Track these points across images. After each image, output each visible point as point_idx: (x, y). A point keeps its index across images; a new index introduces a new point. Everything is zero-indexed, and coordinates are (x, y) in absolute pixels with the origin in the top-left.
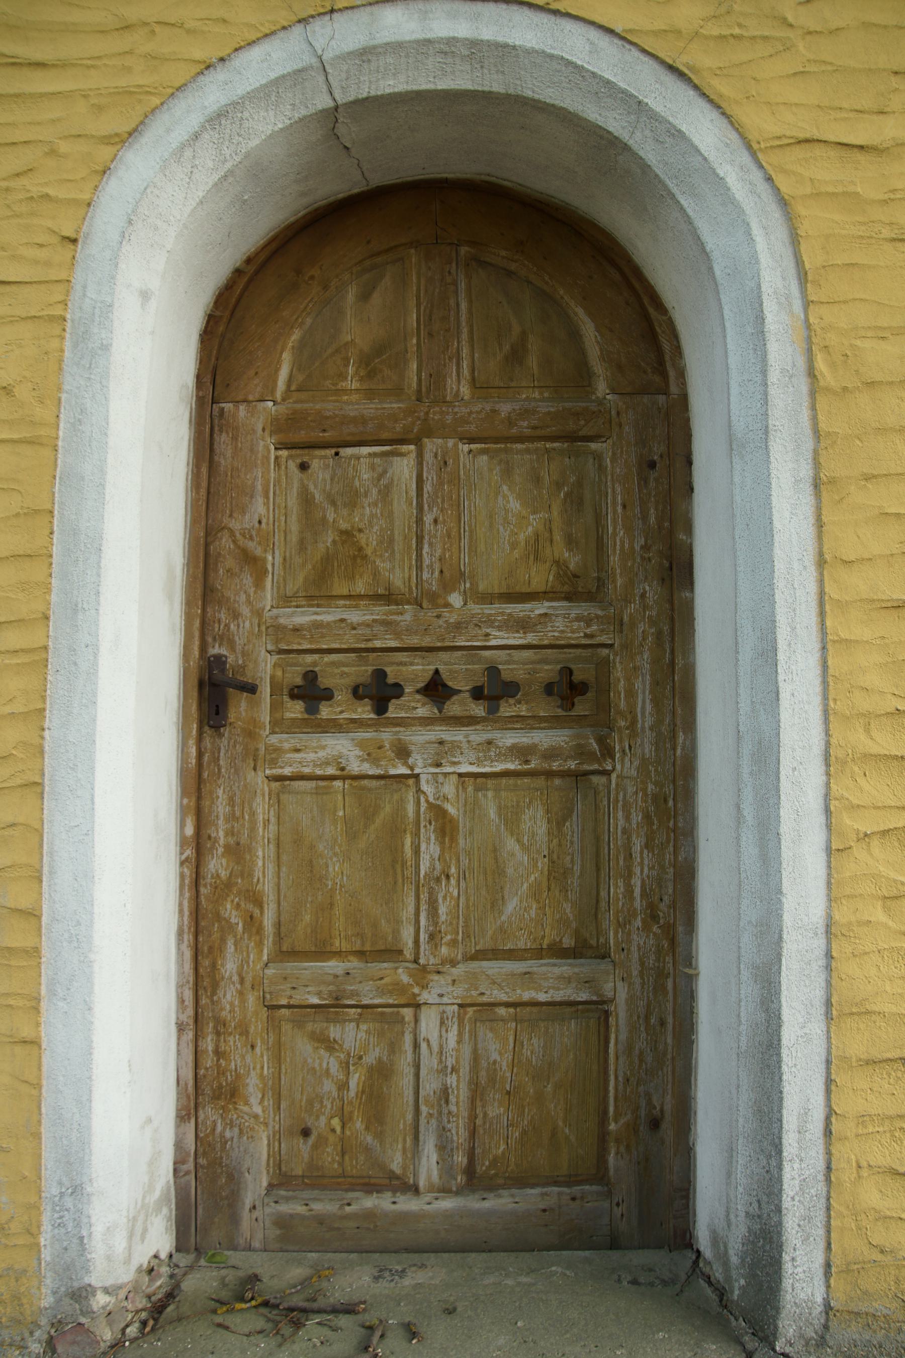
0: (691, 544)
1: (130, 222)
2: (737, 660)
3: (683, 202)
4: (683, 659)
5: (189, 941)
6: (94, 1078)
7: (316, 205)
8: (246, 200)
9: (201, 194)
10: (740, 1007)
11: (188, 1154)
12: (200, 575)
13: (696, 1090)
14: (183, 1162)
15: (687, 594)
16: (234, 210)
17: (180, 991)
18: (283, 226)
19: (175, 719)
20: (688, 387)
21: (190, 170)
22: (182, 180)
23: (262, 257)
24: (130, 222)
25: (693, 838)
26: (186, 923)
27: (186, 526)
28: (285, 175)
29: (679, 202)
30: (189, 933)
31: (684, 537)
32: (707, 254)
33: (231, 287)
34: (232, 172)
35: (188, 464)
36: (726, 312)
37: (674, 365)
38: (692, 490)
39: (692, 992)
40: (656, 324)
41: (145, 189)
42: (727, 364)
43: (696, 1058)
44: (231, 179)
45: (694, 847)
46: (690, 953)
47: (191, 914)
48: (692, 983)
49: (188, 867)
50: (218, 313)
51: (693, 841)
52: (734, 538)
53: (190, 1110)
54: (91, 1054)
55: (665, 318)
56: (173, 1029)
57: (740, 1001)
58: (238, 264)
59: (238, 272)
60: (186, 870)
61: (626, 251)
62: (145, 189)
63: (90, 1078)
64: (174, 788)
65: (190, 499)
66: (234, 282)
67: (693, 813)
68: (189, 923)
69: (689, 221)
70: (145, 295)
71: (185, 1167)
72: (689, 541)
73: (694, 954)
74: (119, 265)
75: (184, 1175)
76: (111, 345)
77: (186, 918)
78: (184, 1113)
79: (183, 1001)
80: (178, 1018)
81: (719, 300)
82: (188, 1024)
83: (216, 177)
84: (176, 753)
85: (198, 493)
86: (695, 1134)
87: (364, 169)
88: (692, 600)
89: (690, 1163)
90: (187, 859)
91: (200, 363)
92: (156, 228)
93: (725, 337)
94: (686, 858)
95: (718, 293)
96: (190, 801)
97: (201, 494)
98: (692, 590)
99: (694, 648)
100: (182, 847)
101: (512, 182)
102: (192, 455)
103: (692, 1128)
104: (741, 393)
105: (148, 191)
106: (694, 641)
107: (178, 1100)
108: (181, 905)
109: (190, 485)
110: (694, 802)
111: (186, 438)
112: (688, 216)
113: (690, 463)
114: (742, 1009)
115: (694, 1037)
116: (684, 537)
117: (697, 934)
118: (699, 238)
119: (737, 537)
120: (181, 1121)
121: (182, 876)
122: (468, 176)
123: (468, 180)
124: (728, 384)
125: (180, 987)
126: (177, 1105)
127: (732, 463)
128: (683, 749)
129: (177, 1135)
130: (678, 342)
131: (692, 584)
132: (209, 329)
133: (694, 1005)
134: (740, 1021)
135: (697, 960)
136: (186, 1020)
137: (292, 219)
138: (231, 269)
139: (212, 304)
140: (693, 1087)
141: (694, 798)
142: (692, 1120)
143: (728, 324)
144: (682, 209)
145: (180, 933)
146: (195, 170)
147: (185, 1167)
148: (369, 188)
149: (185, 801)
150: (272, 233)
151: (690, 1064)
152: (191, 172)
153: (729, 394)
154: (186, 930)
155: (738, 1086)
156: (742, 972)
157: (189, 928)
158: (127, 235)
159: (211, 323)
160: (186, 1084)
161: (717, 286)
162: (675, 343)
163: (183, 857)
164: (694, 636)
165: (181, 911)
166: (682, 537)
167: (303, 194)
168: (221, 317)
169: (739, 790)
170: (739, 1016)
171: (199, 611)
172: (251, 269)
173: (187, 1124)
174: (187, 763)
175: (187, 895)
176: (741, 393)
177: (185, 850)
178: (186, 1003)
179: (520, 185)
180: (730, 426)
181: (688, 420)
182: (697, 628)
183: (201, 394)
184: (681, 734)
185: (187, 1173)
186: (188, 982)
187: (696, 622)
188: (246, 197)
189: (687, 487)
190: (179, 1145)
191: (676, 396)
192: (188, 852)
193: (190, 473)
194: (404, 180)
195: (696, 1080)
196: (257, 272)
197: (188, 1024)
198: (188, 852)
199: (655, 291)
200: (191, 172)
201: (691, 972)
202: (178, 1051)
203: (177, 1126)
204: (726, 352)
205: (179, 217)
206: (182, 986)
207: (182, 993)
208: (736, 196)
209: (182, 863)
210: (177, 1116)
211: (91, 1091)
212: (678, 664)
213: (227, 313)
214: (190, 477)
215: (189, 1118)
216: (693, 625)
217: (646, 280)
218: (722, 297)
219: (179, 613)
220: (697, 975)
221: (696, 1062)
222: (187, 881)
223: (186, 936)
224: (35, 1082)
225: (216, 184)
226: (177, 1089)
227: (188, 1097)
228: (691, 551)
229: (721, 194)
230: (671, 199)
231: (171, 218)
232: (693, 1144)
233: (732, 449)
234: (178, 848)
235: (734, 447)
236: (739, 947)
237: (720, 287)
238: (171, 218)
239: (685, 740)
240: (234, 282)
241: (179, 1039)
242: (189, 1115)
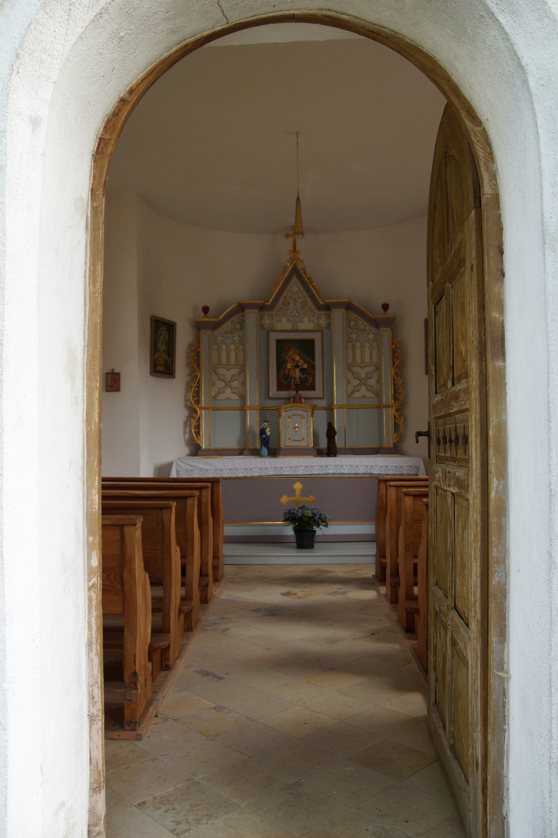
0: (503, 321)
1: (17, 56)
2: (550, 428)
3: (501, 20)
4: (496, 418)
5: (97, 650)
6: (8, 786)
7: (185, 42)
8: (123, 37)
9: (80, 30)
10: (551, 724)
11: (99, 819)
12: (98, 355)
13: (508, 771)
14: (96, 825)
15: (500, 364)
16: (112, 45)
17: (90, 689)
18: (158, 61)
19: (80, 474)
20: (499, 187)
21: (68, 7)
22: (62, 17)
23: (142, 88)
24: (17, 56)
25: (505, 565)
26: (94, 636)
27: (85, 315)
28: (155, 14)
29: (497, 20)
30: (96, 644)
31: (497, 316)
32: (522, 68)
33: (118, 114)
34: (106, 9)
35: (86, 264)
36: (540, 120)
37: (487, 169)
38: (503, 275)
39: (504, 690)
40: (472, 134)
41: (29, 25)
42: (540, 167)
43: (508, 744)
44: (106, 17)
45: (506, 573)
46: (502, 659)
47: (98, 629)
48: (504, 683)
49: (94, 592)
50: (107, 137)
51: (505, 568)
52: (546, 321)
53: (100, 784)
54: (6, 767)
55: (479, 129)
56: (86, 720)
57: (552, 719)
58: (122, 95)
59: (123, 101)
60: (93, 594)
61: (446, 72)
62: (29, 25)
63: (5, 787)
64: (81, 530)
65: (88, 292)
66: (120, 110)
67: (505, 545)
68: (97, 636)
69: (506, 37)
70: (35, 122)
71: (97, 829)
72: (501, 318)
73: (505, 660)
74: (10, 95)
75: (97, 835)
76: (6, 166)
77: (94, 632)
78: (95, 786)
79: (93, 698)
80: (89, 711)
81: (533, 109)
82: (97, 716)
83: (92, 14)
84: (81, 501)
85: (94, 287)
86: (508, 806)
87: (223, 7)
88: (504, 368)
89: (504, 830)
90: (93, 585)
91: (94, 179)
92: (42, 62)
93: (538, 142)
94: (499, 582)
95: (532, 103)
96: (95, 539)
97: (97, 287)
98: (504, 360)
99: (505, 408)
100: (89, 575)
101: (349, 15)
102: (89, 255)
103: (505, 800)
104: (553, 193)
105: (32, 27)
106: (505, 402)
107: (91, 776)
108: (89, 622)
109: (87, 281)
110: (505, 536)
111: (83, 242)
112: (506, 33)
113: (501, 252)
114: (554, 726)
115: (505, 727)
116: (497, 316)
117: (508, 644)
118: (515, 53)
119: (549, 320)
120: (93, 792)
121: (90, 599)
122: (312, 12)
123: (312, 15)
124: (541, 185)
125: (91, 686)
126: (90, 780)
127: (544, 255)
128: (497, 492)
129: (90, 803)
130: (491, 149)
131: (503, 354)
132: (100, 150)
133: (506, 700)
134: (552, 736)
135: (508, 665)
136: (96, 712)
137: (166, 55)
138: (117, 99)
139: (102, 129)
140: (505, 767)
141: (505, 532)
142: (505, 795)
143: (541, 131)
144: (501, 28)
145: (90, 644)
146: (73, 8)
147: (97, 829)
148: (229, 25)
149: (91, 539)
150: (150, 67)
151: (502, 749)
152: (70, 10)
153: (542, 194)
154: (94, 642)
155: (551, 791)
156: (553, 695)
157: (97, 640)
158: (15, 68)
159: (102, 145)
160: (97, 763)
161: (531, 97)
162: (488, 150)
163: (91, 584)
164: (505, 397)
165: (90, 627)
166: (495, 315)
167: (173, 32)
168: (110, 139)
169: (551, 540)
170: (550, 731)
171: (98, 384)
172: (134, 98)
173: (99, 794)
174: (92, 508)
175: (94, 614)
176: (553, 193)
177: (92, 578)
178: (96, 699)
179: (356, 17)
180: (543, 223)
181: (500, 216)
182: (508, 391)
183: (95, 204)
184: (495, 480)
185: (99, 834)
186: (97, 683)
187: (507, 387)
188: (122, 34)
189: (499, 273)
190: (92, 812)
191: (489, 196)
192: (94, 580)
193: (88, 271)
194: (258, 17)
195: (508, 762)
196: (138, 101)
197: (97, 716)
198: (94, 580)
199: (471, 106)
200: (70, 10)
201: (504, 675)
202: (90, 737)
203: (91, 796)
204: (539, 156)
205: (62, 52)
206: (92, 686)
207: (92, 691)
208: (552, 9)
209: (90, 589)
210: (90, 789)
211: (6, 798)
212: (492, 422)
213: (115, 136)
214: (88, 274)
215: (100, 790)
216: (505, 389)
217: (464, 97)
218: (535, 106)
219: (81, 387)
220: (510, 678)
221: (508, 748)
222: (94, 603)
223: (94, 647)
224: (295, 279)
225: (93, 21)
226: (90, 767)
227: (99, 773)
228: (503, 327)
229: (538, 9)
230: (491, 18)
231: (55, 52)
232: (507, 815)
233: (544, 243)
234: (86, 577)
235: (547, 241)
236: (551, 673)
237: (534, 98)
238: (55, 52)
239: (498, 485)
240: (120, 110)
241: (90, 727)
242: (99, 787)
